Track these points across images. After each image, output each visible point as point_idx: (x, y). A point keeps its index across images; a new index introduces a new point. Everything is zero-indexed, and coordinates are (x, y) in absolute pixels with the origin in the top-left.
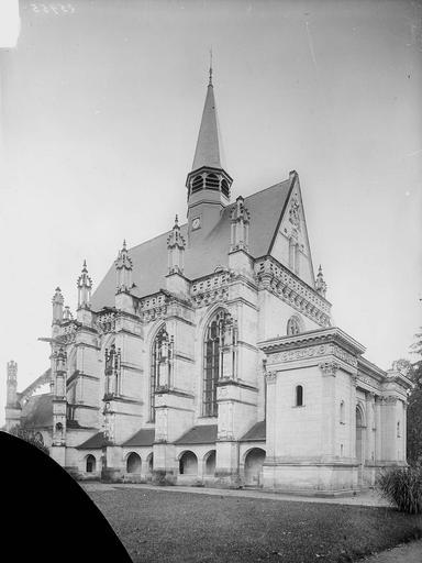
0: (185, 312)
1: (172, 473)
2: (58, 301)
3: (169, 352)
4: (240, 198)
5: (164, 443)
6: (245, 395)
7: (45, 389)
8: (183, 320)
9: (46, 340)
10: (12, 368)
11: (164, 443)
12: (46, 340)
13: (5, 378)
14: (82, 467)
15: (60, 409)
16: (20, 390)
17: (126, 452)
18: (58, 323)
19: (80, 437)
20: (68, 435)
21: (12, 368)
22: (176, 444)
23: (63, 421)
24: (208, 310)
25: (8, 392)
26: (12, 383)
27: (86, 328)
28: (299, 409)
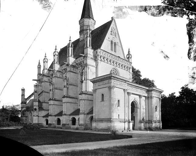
0: (74, 69)
1: (68, 125)
2: (39, 67)
3: (67, 84)
4: (114, 12)
5: (65, 115)
6: (56, 103)
7: (33, 98)
8: (72, 72)
9: (35, 80)
10: (23, 90)
11: (65, 115)
12: (35, 80)
13: (21, 94)
14: (44, 123)
15: (36, 104)
16: (26, 97)
17: (56, 118)
18: (39, 74)
19: (44, 113)
20: (39, 112)
21: (23, 90)
22: (55, 116)
23: (37, 108)
24: (81, 68)
25: (22, 98)
26: (23, 95)
27: (46, 76)
28: (103, 103)
